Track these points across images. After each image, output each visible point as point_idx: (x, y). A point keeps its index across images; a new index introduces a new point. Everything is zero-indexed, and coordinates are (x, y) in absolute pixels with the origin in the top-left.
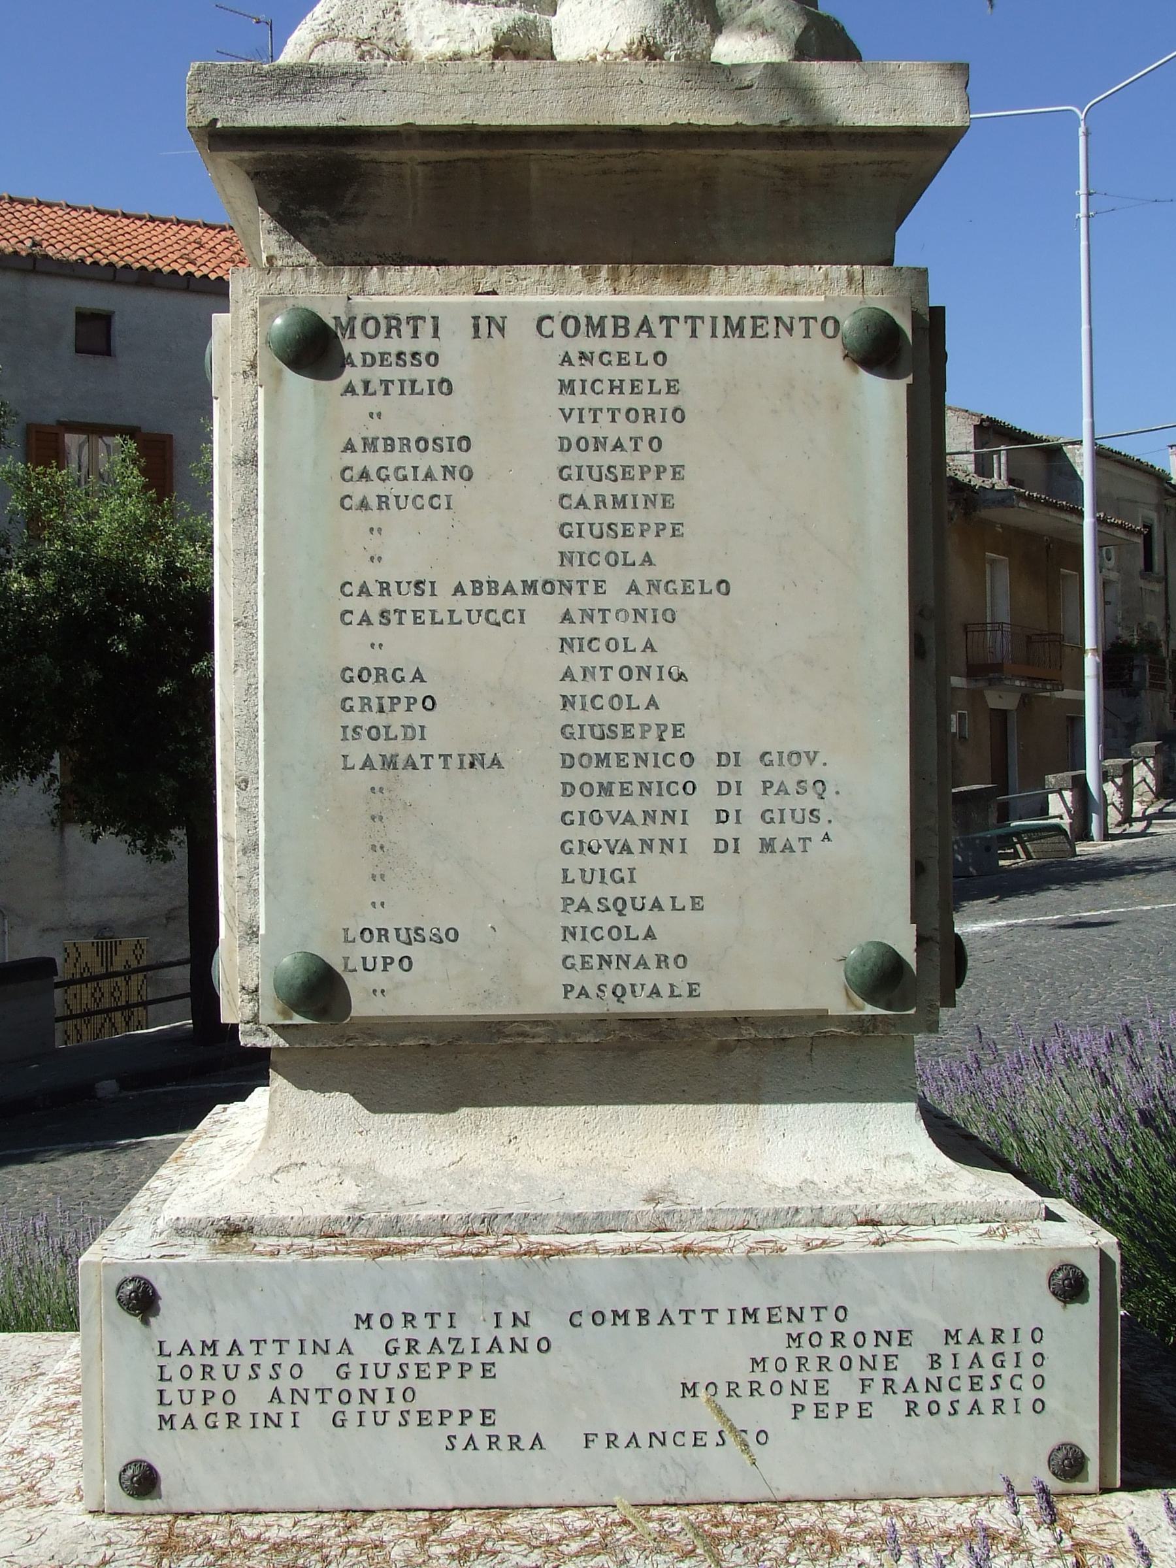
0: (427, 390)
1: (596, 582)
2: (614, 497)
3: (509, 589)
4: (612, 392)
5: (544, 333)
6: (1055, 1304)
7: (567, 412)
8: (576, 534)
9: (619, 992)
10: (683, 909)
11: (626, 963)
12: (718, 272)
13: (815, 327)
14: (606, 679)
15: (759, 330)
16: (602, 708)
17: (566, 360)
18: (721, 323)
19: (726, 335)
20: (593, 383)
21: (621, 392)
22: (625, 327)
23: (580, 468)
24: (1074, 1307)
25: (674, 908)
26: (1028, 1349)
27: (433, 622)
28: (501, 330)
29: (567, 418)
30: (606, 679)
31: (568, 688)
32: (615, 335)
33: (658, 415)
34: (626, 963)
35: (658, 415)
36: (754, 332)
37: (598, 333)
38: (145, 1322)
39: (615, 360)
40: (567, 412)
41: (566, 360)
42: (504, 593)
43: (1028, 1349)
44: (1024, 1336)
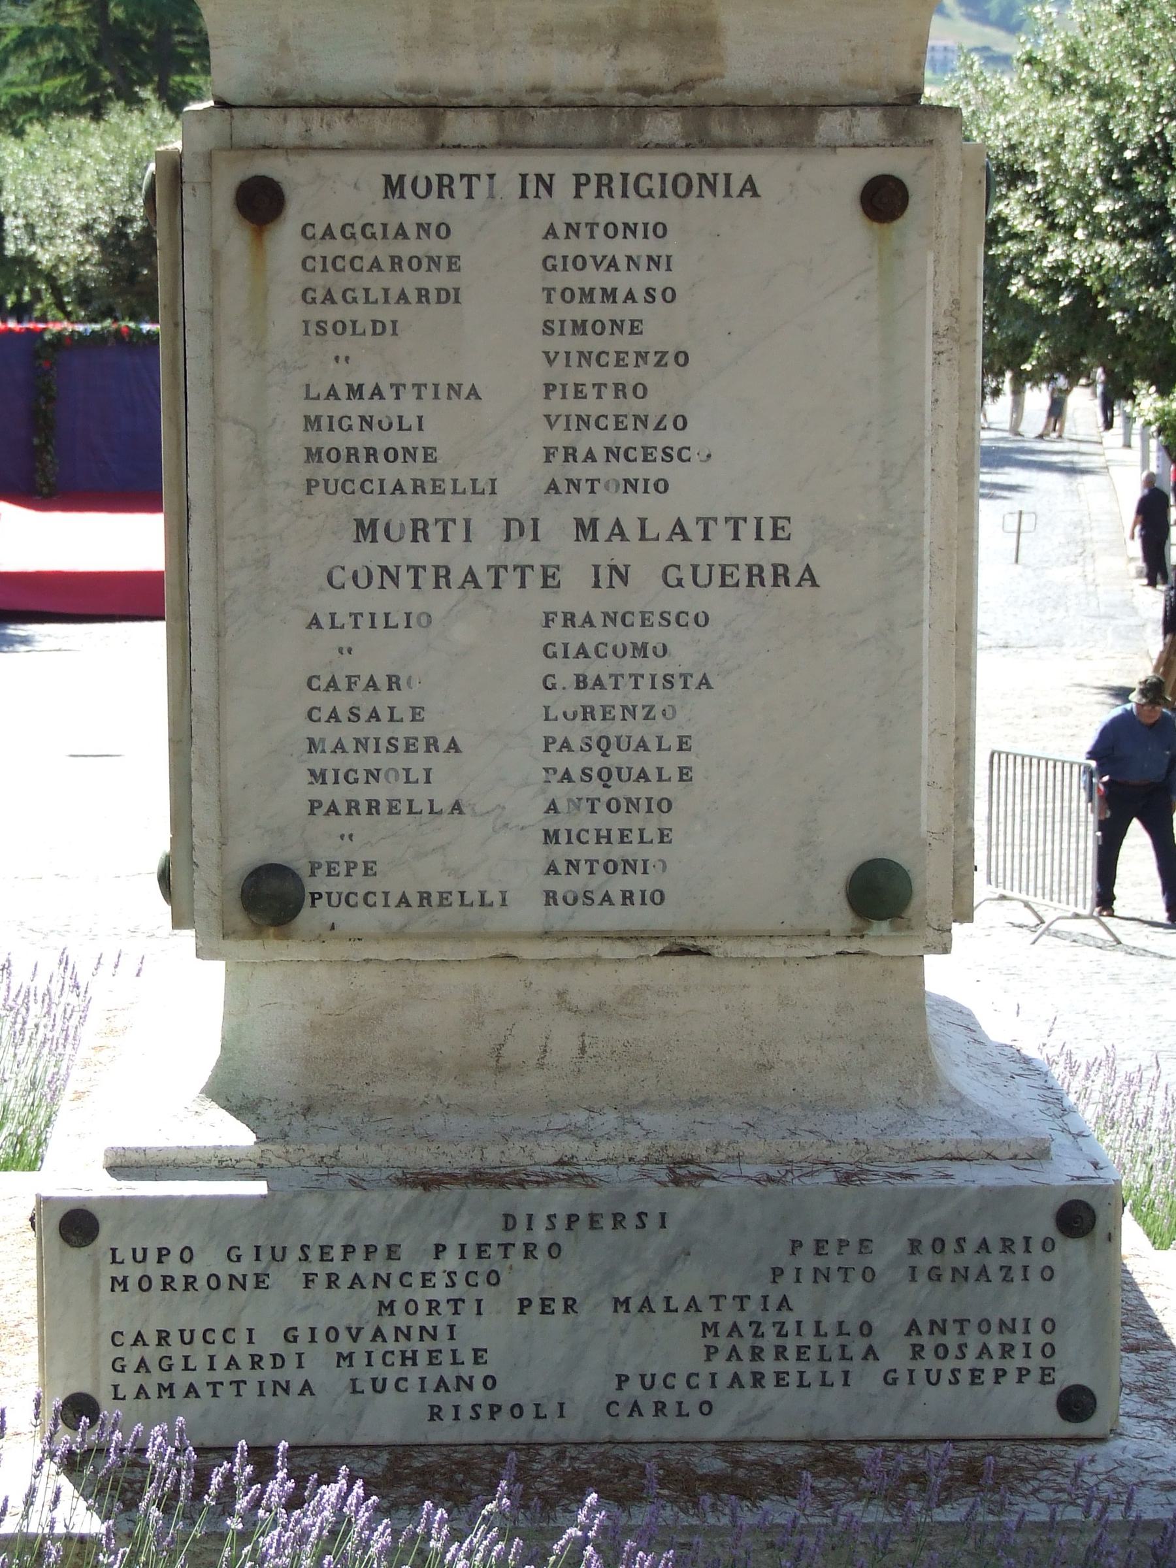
0: (381, 299)
4: (598, 842)
9: (605, 776)
14: (592, 491)
17: (552, 869)
21: (609, 842)
24: (1054, 1412)
26: (1037, 1338)
27: (367, 301)
29: (551, 362)
30: (592, 491)
31: (552, 883)
33: (637, 898)
35: (637, 898)
38: (39, 1197)
39: (612, 425)
40: (552, 355)
41: (552, 869)
43: (1037, 1338)
44: (1035, 1326)
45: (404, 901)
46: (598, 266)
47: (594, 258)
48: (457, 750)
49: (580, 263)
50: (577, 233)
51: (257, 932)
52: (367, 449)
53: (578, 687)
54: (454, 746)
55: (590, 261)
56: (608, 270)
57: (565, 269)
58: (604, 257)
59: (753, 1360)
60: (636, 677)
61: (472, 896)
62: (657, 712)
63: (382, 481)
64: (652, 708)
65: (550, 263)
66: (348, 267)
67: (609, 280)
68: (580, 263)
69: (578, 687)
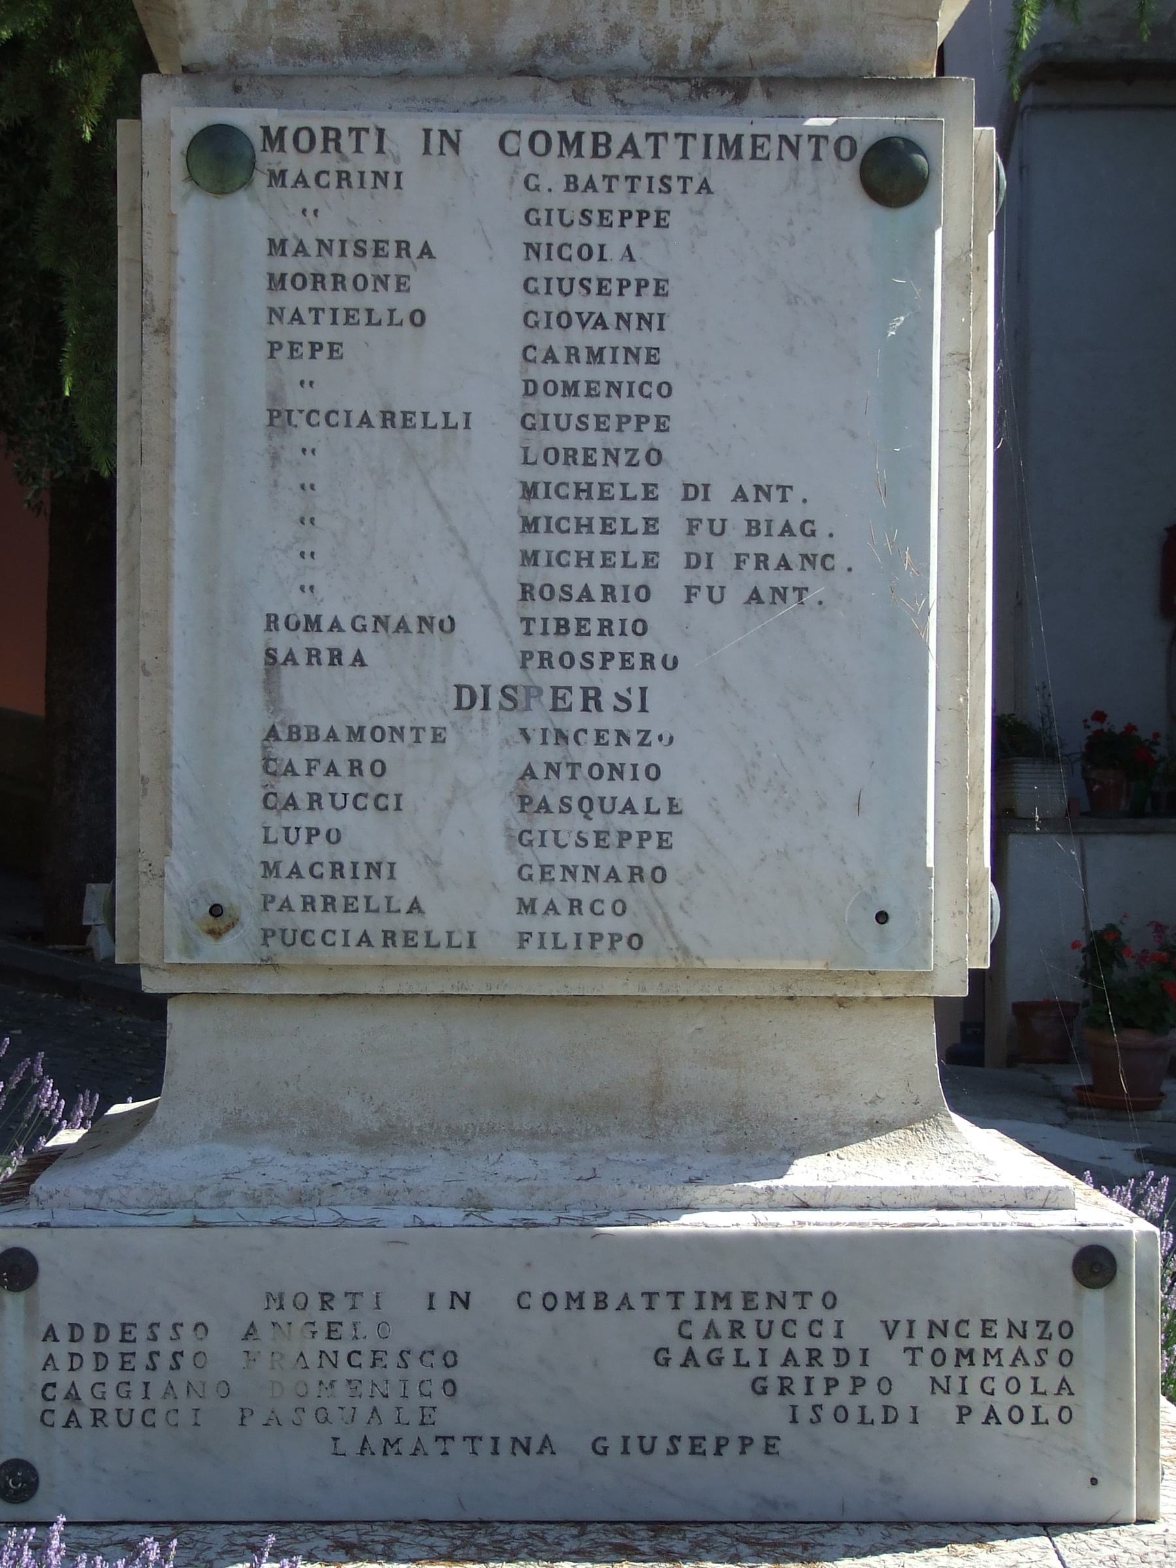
1: (693, 1438)
2: (590, 349)
3: (332, 735)
5: (507, 149)
6: (891, 921)
7: (891, 1325)
8: (544, 221)
10: (658, 812)
11: (595, 875)
12: (686, 117)
13: (826, 150)
15: (759, 151)
16: (602, 913)
18: (715, 142)
19: (720, 157)
20: (356, 797)
22: (607, 145)
23: (548, 280)
25: (648, 812)
28: (455, 146)
32: (595, 154)
34: (595, 875)
36: (754, 152)
37: (574, 152)
42: (585, 191)
45: (365, 420)
46: (584, 325)
47: (579, 314)
48: (431, 256)
49: (564, 320)
50: (557, 774)
51: (199, 105)
52: (325, 897)
53: (567, 190)
54: (426, 251)
55: (575, 318)
56: (594, 328)
57: (548, 326)
58: (591, 314)
59: (810, 1365)
60: (633, 179)
61: (439, 936)
62: (653, 737)
63: (348, 413)
64: (648, 732)
65: (532, 319)
66: (323, 422)
67: (597, 339)
68: (564, 320)
69: (567, 190)
